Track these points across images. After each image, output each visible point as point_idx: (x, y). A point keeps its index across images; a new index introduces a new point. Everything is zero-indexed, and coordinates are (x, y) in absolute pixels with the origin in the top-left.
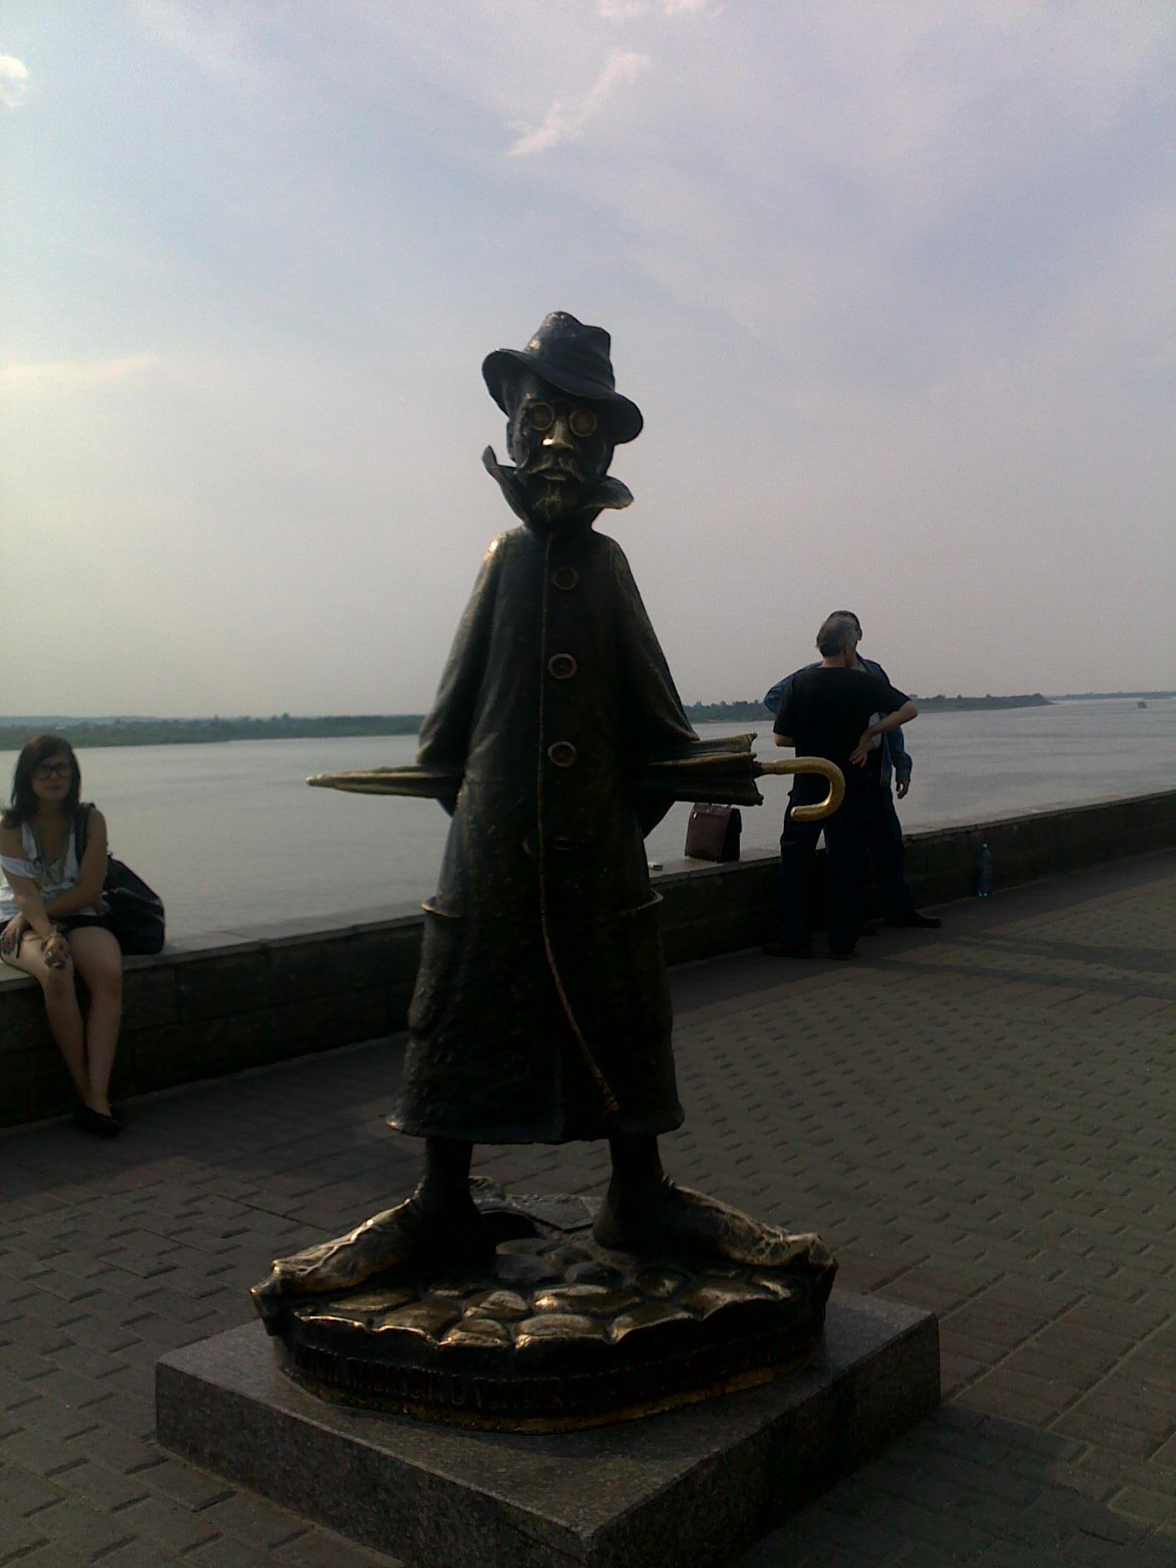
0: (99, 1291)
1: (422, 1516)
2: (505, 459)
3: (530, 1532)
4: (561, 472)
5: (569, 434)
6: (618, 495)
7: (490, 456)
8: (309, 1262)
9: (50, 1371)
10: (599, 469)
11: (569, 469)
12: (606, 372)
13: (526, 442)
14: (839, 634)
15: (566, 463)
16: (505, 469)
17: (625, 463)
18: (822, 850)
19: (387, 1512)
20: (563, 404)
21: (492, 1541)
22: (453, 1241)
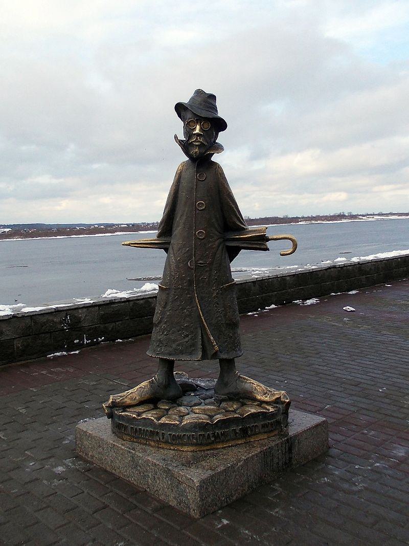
0: (65, 407)
1: (150, 475)
3: (180, 480)
5: (201, 129)
6: (219, 148)
7: (176, 137)
8: (121, 397)
9: (47, 430)
12: (215, 109)
13: (189, 133)
14: (180, 109)
15: (200, 138)
17: (222, 138)
19: (140, 473)
20: (202, 122)
21: (169, 482)
22: (168, 393)
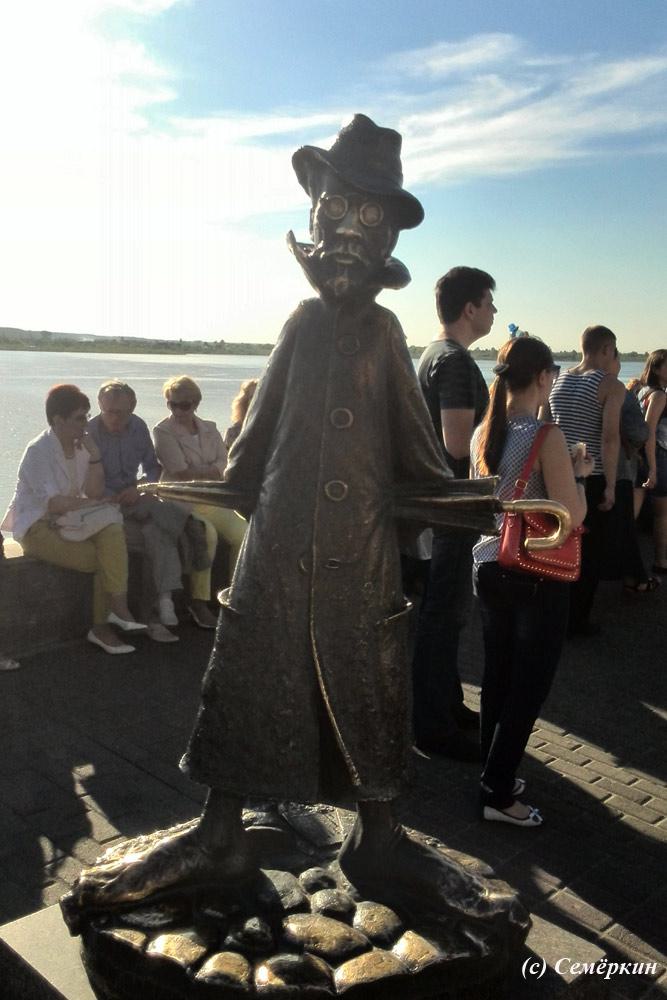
2: (305, 236)
4: (347, 256)
7: (291, 237)
10: (383, 253)
11: (356, 254)
12: (394, 170)
13: (326, 226)
15: (354, 248)
16: (307, 247)
18: (99, 419)
